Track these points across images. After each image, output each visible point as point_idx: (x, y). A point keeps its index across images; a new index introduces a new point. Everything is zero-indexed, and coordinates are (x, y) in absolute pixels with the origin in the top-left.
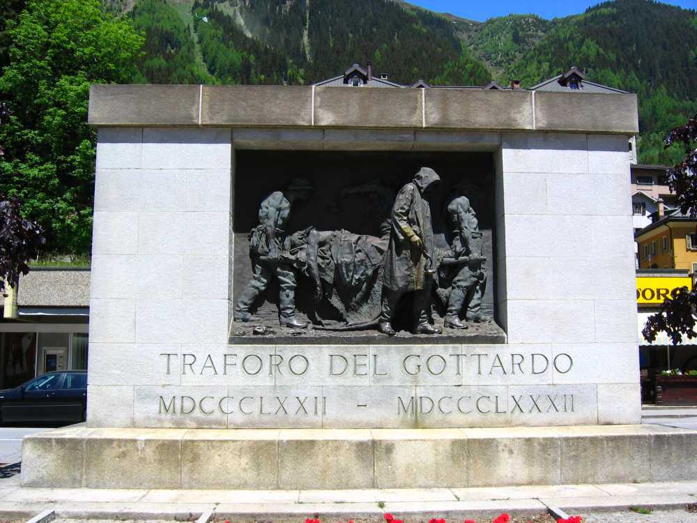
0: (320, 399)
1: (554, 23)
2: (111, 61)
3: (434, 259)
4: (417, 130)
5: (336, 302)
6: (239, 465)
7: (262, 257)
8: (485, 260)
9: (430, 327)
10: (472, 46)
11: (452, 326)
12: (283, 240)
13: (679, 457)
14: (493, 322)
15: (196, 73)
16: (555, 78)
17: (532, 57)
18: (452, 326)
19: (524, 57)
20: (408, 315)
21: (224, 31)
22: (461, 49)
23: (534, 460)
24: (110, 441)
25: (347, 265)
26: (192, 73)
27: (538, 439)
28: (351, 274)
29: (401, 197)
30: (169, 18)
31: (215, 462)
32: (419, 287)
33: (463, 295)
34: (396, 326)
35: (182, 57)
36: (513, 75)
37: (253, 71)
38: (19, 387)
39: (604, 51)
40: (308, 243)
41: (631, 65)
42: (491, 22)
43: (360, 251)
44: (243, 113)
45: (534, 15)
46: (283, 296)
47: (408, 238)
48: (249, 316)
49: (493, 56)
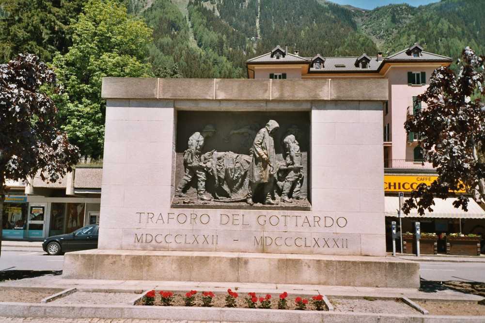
0: (215, 237)
1: (420, 8)
2: (133, 44)
3: (275, 166)
4: (267, 101)
5: (226, 188)
6: (171, 268)
7: (189, 165)
8: (302, 168)
9: (272, 201)
10: (364, 26)
11: (284, 201)
12: (200, 157)
13: (403, 275)
14: (307, 200)
15: (190, 47)
16: (403, 51)
17: (404, 32)
18: (284, 201)
19: (399, 32)
20: (261, 195)
21: (207, 20)
22: (357, 29)
23: (321, 271)
24: (108, 256)
25: (231, 169)
26: (188, 47)
27: (324, 261)
28: (233, 174)
29: (258, 135)
30: (173, 12)
31: (159, 267)
32: (266, 181)
33: (291, 186)
34: (255, 201)
35: (181, 37)
36: (391, 44)
37: (225, 45)
38: (72, 233)
39: (454, 26)
40: (212, 158)
41: (471, 35)
42: (377, 9)
43: (238, 162)
44: (180, 93)
45: (406, 4)
46: (198, 185)
47: (261, 156)
48: (182, 194)
49: (378, 32)
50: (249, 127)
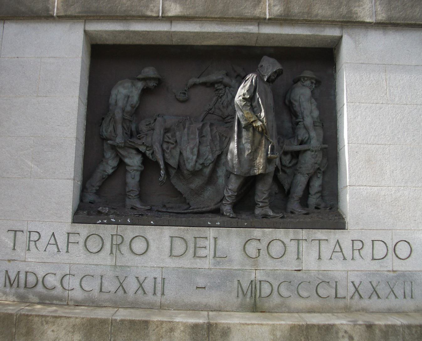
27: (380, 325)
50: (225, 72)
